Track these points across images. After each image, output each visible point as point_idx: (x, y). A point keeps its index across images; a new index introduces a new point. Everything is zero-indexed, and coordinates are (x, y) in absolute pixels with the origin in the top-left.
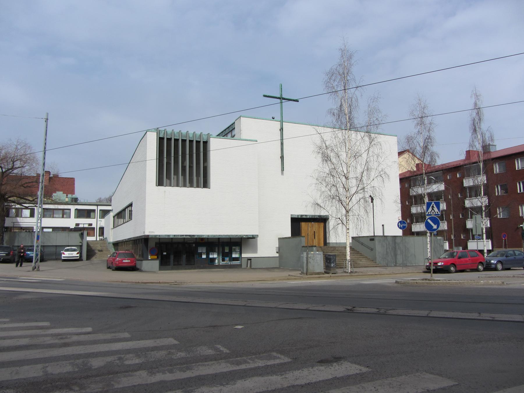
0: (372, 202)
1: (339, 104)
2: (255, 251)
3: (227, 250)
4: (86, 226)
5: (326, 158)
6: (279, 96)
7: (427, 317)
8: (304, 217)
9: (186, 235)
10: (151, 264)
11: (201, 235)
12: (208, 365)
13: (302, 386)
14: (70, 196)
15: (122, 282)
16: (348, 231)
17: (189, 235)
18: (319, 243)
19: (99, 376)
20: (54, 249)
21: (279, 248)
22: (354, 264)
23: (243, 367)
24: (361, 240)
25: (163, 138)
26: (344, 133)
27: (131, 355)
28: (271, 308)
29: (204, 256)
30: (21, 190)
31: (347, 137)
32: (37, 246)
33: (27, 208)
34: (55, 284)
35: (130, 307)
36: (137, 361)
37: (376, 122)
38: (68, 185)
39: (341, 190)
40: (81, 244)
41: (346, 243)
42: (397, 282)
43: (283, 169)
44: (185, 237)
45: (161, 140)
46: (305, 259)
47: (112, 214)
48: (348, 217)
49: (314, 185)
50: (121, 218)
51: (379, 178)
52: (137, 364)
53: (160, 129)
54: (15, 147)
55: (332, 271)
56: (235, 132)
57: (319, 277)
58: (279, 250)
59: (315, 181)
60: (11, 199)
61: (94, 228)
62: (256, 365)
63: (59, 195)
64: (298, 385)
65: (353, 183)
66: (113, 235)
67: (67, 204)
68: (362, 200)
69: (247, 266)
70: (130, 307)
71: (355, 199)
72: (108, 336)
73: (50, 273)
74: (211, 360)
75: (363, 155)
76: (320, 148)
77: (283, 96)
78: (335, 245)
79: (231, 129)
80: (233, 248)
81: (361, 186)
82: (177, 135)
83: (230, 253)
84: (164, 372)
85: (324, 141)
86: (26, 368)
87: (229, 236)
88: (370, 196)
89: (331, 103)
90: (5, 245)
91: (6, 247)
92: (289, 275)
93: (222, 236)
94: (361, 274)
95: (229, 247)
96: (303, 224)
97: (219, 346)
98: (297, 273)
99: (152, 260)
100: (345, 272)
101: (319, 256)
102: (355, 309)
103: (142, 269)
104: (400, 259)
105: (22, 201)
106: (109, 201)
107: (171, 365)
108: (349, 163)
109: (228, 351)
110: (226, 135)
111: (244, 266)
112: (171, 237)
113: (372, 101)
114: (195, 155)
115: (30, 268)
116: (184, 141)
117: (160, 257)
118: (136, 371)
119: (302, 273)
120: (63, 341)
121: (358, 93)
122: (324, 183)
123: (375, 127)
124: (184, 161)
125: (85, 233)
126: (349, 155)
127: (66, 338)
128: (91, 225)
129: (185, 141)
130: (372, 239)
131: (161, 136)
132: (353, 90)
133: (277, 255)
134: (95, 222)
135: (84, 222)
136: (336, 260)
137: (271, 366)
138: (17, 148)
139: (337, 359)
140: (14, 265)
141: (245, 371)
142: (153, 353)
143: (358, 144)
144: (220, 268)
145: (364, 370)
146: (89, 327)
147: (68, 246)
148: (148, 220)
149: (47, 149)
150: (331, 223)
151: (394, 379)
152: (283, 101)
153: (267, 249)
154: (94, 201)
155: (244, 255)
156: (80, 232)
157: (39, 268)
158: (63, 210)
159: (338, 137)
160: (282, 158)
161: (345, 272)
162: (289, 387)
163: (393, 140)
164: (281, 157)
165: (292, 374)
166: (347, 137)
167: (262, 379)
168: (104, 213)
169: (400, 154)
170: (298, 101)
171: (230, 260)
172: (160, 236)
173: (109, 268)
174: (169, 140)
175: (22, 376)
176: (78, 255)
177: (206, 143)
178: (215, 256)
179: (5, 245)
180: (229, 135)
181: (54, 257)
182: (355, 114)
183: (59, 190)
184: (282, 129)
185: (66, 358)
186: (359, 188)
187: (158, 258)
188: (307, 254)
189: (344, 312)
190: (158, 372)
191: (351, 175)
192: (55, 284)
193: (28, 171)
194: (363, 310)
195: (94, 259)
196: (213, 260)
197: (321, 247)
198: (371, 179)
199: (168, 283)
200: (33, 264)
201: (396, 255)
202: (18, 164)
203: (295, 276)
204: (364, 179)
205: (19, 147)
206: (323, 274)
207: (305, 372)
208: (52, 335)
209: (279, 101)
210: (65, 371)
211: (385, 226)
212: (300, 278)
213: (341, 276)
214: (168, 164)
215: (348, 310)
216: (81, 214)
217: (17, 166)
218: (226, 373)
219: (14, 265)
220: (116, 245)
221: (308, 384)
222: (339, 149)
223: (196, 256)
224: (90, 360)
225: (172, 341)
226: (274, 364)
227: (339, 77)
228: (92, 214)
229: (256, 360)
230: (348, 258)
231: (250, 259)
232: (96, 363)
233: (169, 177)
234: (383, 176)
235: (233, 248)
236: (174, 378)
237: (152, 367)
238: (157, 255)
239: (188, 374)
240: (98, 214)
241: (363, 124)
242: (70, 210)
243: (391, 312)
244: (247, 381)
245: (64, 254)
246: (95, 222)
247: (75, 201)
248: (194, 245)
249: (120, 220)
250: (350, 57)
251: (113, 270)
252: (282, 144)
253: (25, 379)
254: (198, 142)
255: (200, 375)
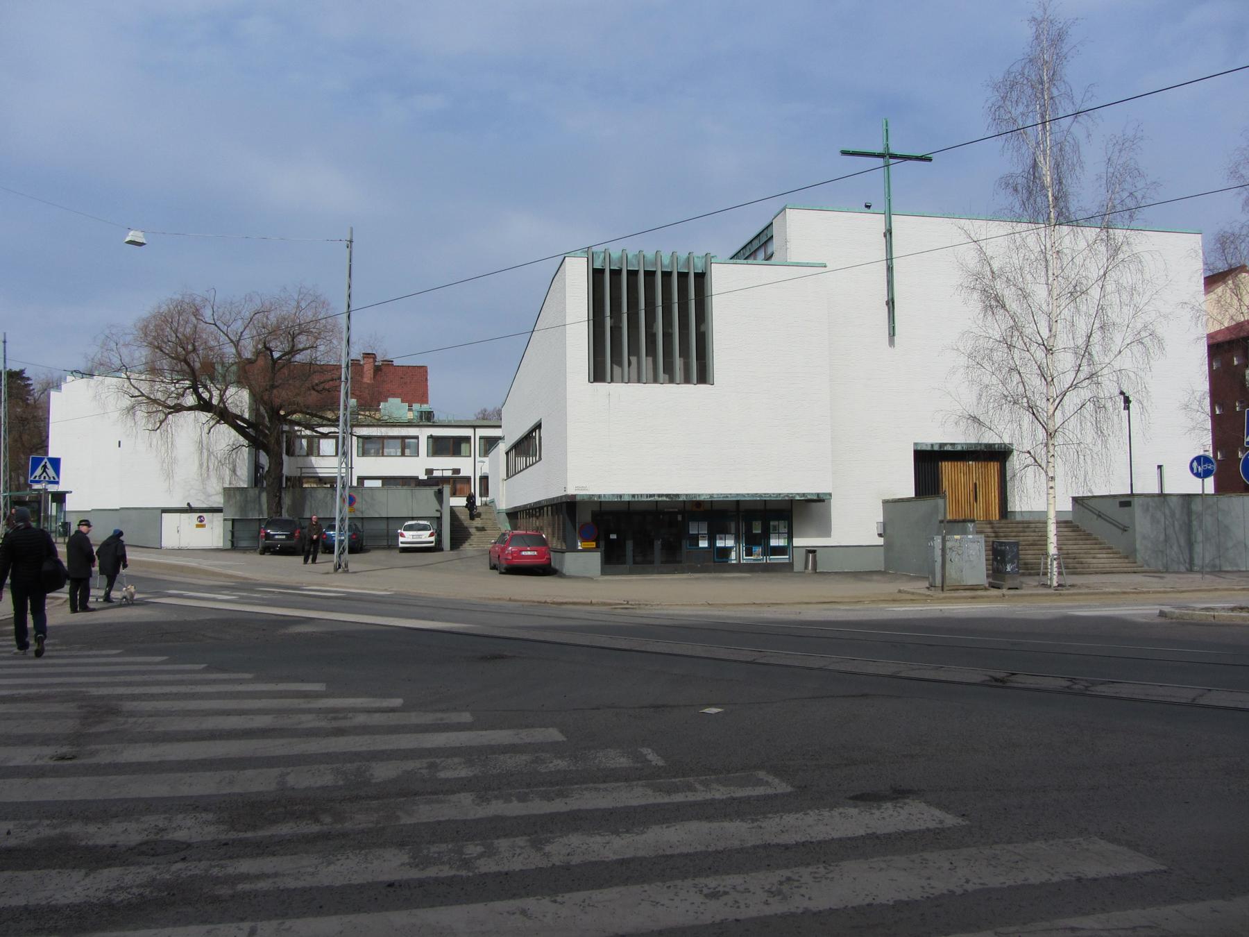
0: (1127, 408)
1: (1029, 162)
2: (826, 531)
3: (757, 530)
4: (449, 474)
5: (994, 303)
6: (880, 150)
7: (1192, 705)
8: (949, 448)
9: (659, 495)
10: (584, 561)
11: (695, 495)
12: (606, 789)
13: (787, 847)
14: (416, 406)
15: (510, 600)
16: (1051, 484)
17: (667, 495)
18: (987, 511)
19: (378, 798)
20: (383, 525)
21: (885, 524)
22: (1070, 565)
23: (679, 798)
24: (1092, 503)
25: (602, 271)
26: (1043, 235)
27: (456, 760)
28: (811, 669)
29: (703, 544)
30: (313, 397)
31: (1048, 246)
32: (342, 520)
33: (325, 436)
34: (371, 601)
35: (502, 657)
36: (464, 773)
37: (1131, 203)
38: (412, 382)
39: (1036, 382)
40: (438, 515)
41: (1045, 513)
42: (1162, 614)
43: (892, 333)
44: (657, 498)
45: (597, 275)
46: (938, 552)
47: (502, 447)
48: (1051, 448)
49: (962, 370)
50: (527, 454)
51: (1136, 348)
52: (462, 778)
53: (594, 249)
54: (294, 304)
55: (1009, 583)
56: (775, 245)
57: (974, 598)
58: (885, 531)
59: (963, 360)
60: (295, 417)
61: (468, 479)
62: (709, 796)
63: (394, 407)
64: (778, 845)
65: (1065, 362)
66: (508, 494)
67: (409, 424)
68: (1090, 406)
69: (806, 567)
70: (502, 657)
71: (1072, 400)
72: (428, 718)
73: (371, 577)
74: (617, 780)
75: (1091, 292)
76: (978, 277)
77: (892, 151)
78: (1027, 518)
79: (764, 239)
80: (772, 523)
81: (1085, 370)
82: (635, 262)
83: (766, 536)
84: (508, 800)
85: (986, 260)
86: (250, 773)
87: (761, 495)
88: (1122, 393)
89: (1002, 160)
90: (285, 515)
91: (286, 521)
92: (900, 591)
93: (743, 495)
94: (1087, 591)
95: (765, 522)
96: (946, 467)
97: (645, 751)
98: (920, 586)
99: (584, 550)
100: (1045, 585)
101: (975, 545)
102: (1013, 678)
103: (564, 571)
104: (1204, 553)
105: (315, 420)
106: (491, 418)
107: (528, 785)
108: (1056, 311)
109: (661, 763)
110: (753, 254)
111: (798, 566)
112: (626, 499)
113: (1118, 147)
114: (676, 306)
115: (330, 567)
116: (650, 275)
117: (602, 543)
118: (453, 792)
119: (932, 586)
120: (335, 724)
121: (1078, 130)
122: (986, 364)
123: (1127, 214)
124: (652, 322)
125: (447, 489)
126: (1055, 294)
127: (345, 718)
128: (457, 471)
129: (653, 273)
130: (1125, 502)
131: (598, 265)
132: (1065, 123)
133: (881, 541)
134: (464, 465)
135: (444, 465)
136: (1018, 554)
137: (740, 800)
138: (298, 307)
139: (899, 794)
140: (301, 559)
141: (678, 807)
142: (502, 757)
143: (1078, 261)
144: (741, 572)
145: (950, 820)
146: (398, 697)
147: (413, 519)
148: (573, 460)
149: (352, 308)
150: (1016, 462)
151: (1010, 847)
152: (892, 161)
153: (855, 525)
154: (471, 417)
155: (797, 542)
156: (436, 488)
157: (346, 566)
158: (403, 438)
159: (1025, 246)
160: (891, 303)
161: (1045, 585)
162: (755, 847)
163: (1193, 243)
164: (887, 303)
165: (777, 820)
166: (1048, 246)
167: (705, 826)
168: (490, 444)
169: (1212, 281)
170: (930, 160)
171: (764, 554)
172: (600, 496)
173: (494, 567)
174: (616, 274)
175: (237, 789)
176: (432, 539)
177: (701, 277)
178: (730, 543)
179: (285, 515)
180: (761, 255)
181: (385, 543)
182: (1071, 185)
183: (394, 396)
184: (889, 233)
185: (328, 758)
186: (1081, 376)
187: (598, 546)
188: (944, 541)
189: (982, 684)
190: (496, 798)
191: (1063, 340)
192: (371, 601)
193: (323, 355)
194: (1031, 682)
195: (467, 548)
196: (726, 552)
197: (990, 523)
198: (1116, 349)
199: (610, 604)
200: (335, 557)
201: (1190, 545)
202: (302, 341)
203: (913, 594)
204: (1096, 350)
205: (303, 305)
206: (986, 589)
207: (812, 817)
208: (319, 711)
209: (880, 161)
210: (318, 785)
211: (1165, 469)
212: (925, 599)
213: (1031, 595)
214: (616, 330)
215: (996, 680)
216: (442, 447)
217: (301, 346)
218: (635, 808)
219: (301, 559)
220: (513, 515)
221: (803, 844)
222: (1029, 277)
223: (684, 542)
224: (374, 764)
225: (554, 735)
226: (749, 797)
227: (1029, 91)
228: (464, 446)
229: (714, 786)
230: (1052, 550)
231: (812, 551)
232: (383, 772)
233: (616, 359)
234: (1147, 341)
235: (772, 523)
236: (524, 813)
237: (483, 788)
238: (597, 541)
239: (558, 806)
240: (476, 445)
241: (1093, 209)
242: (417, 438)
243: (1100, 690)
244: (673, 829)
245: (402, 535)
246: (464, 465)
247: (427, 419)
248: (680, 518)
249: (518, 459)
250: (1058, 39)
251: (501, 573)
252: (890, 269)
253: (241, 795)
254: (683, 276)
255: (579, 810)
